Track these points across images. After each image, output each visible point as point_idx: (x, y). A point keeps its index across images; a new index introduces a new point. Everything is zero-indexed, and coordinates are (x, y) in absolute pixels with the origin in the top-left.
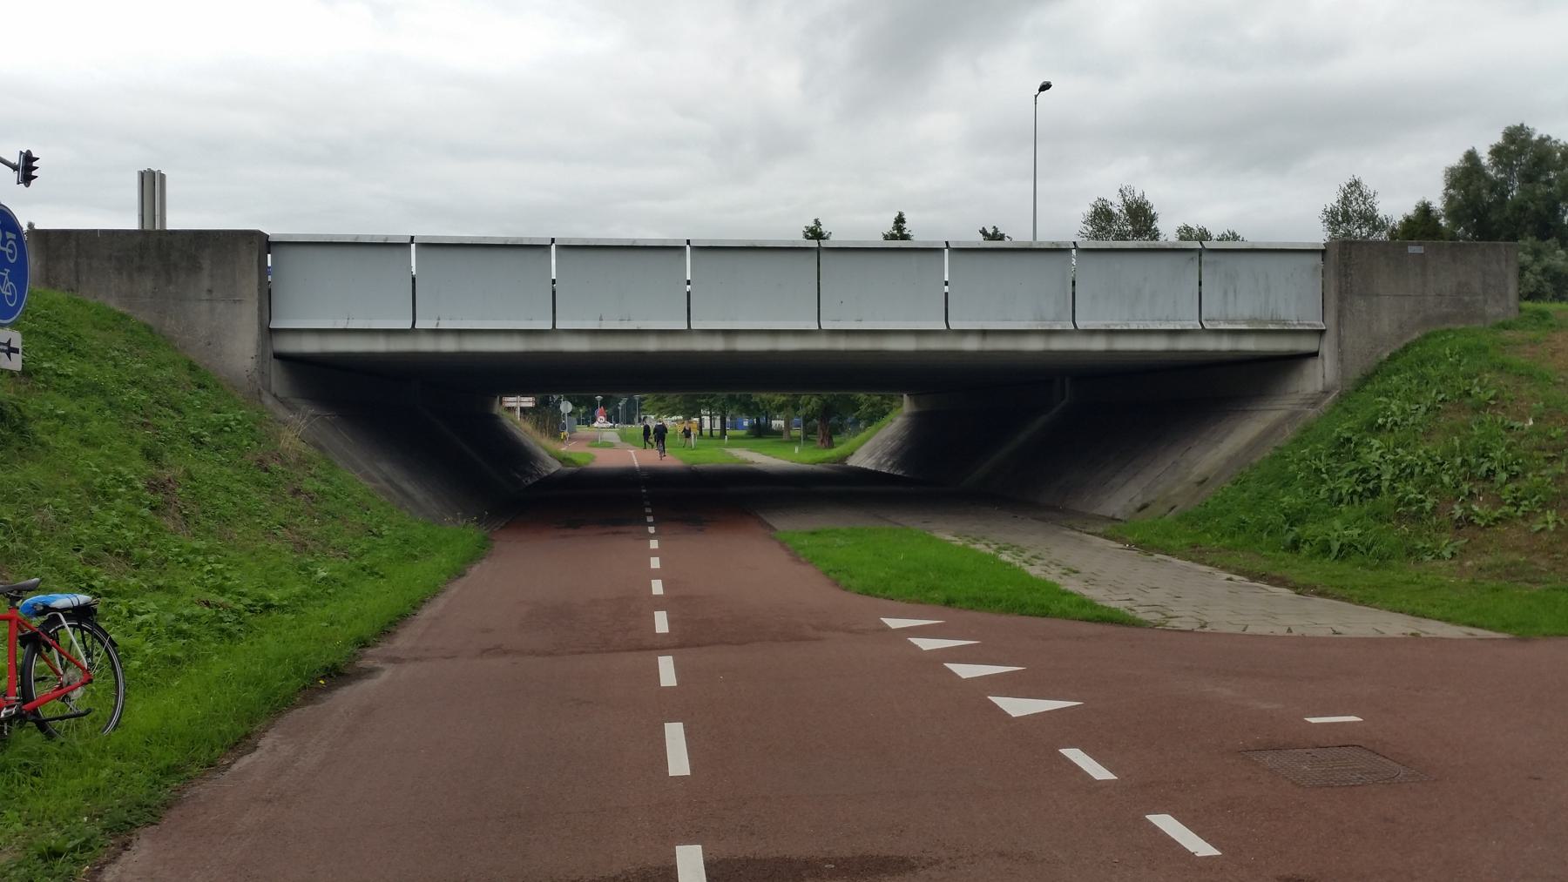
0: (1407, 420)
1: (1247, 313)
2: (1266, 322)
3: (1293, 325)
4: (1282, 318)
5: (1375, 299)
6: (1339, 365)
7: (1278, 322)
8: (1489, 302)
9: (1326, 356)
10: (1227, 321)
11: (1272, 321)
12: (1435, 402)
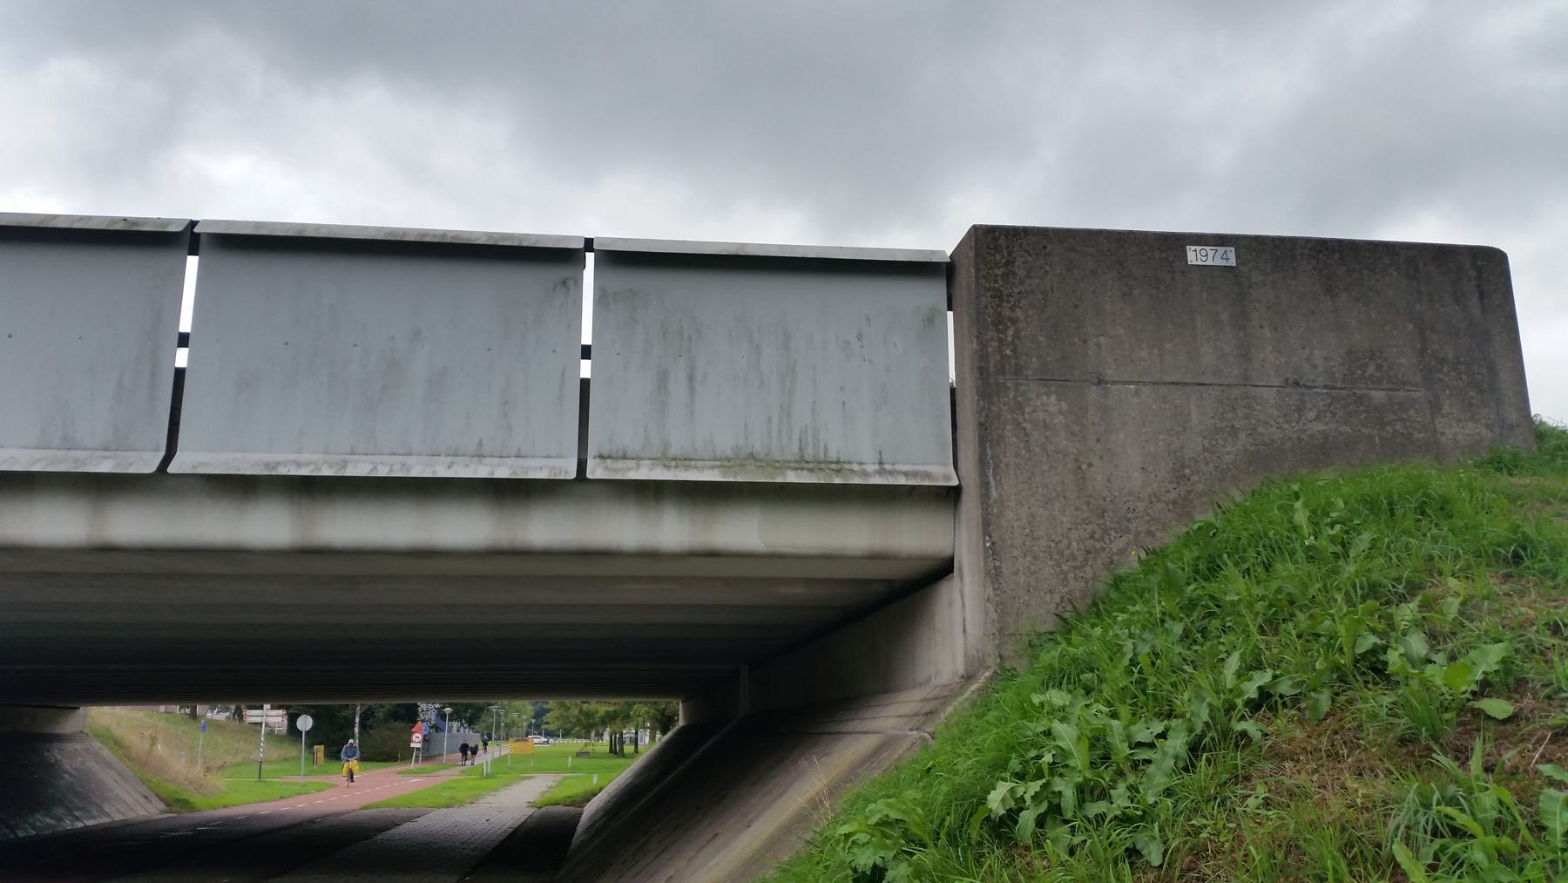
0: (1104, 795)
1: (726, 443)
2: (784, 465)
3: (865, 474)
4: (833, 455)
5: (1093, 393)
6: (990, 591)
7: (818, 465)
8: (1446, 409)
9: (966, 570)
10: (666, 460)
11: (801, 463)
12: (1231, 707)
